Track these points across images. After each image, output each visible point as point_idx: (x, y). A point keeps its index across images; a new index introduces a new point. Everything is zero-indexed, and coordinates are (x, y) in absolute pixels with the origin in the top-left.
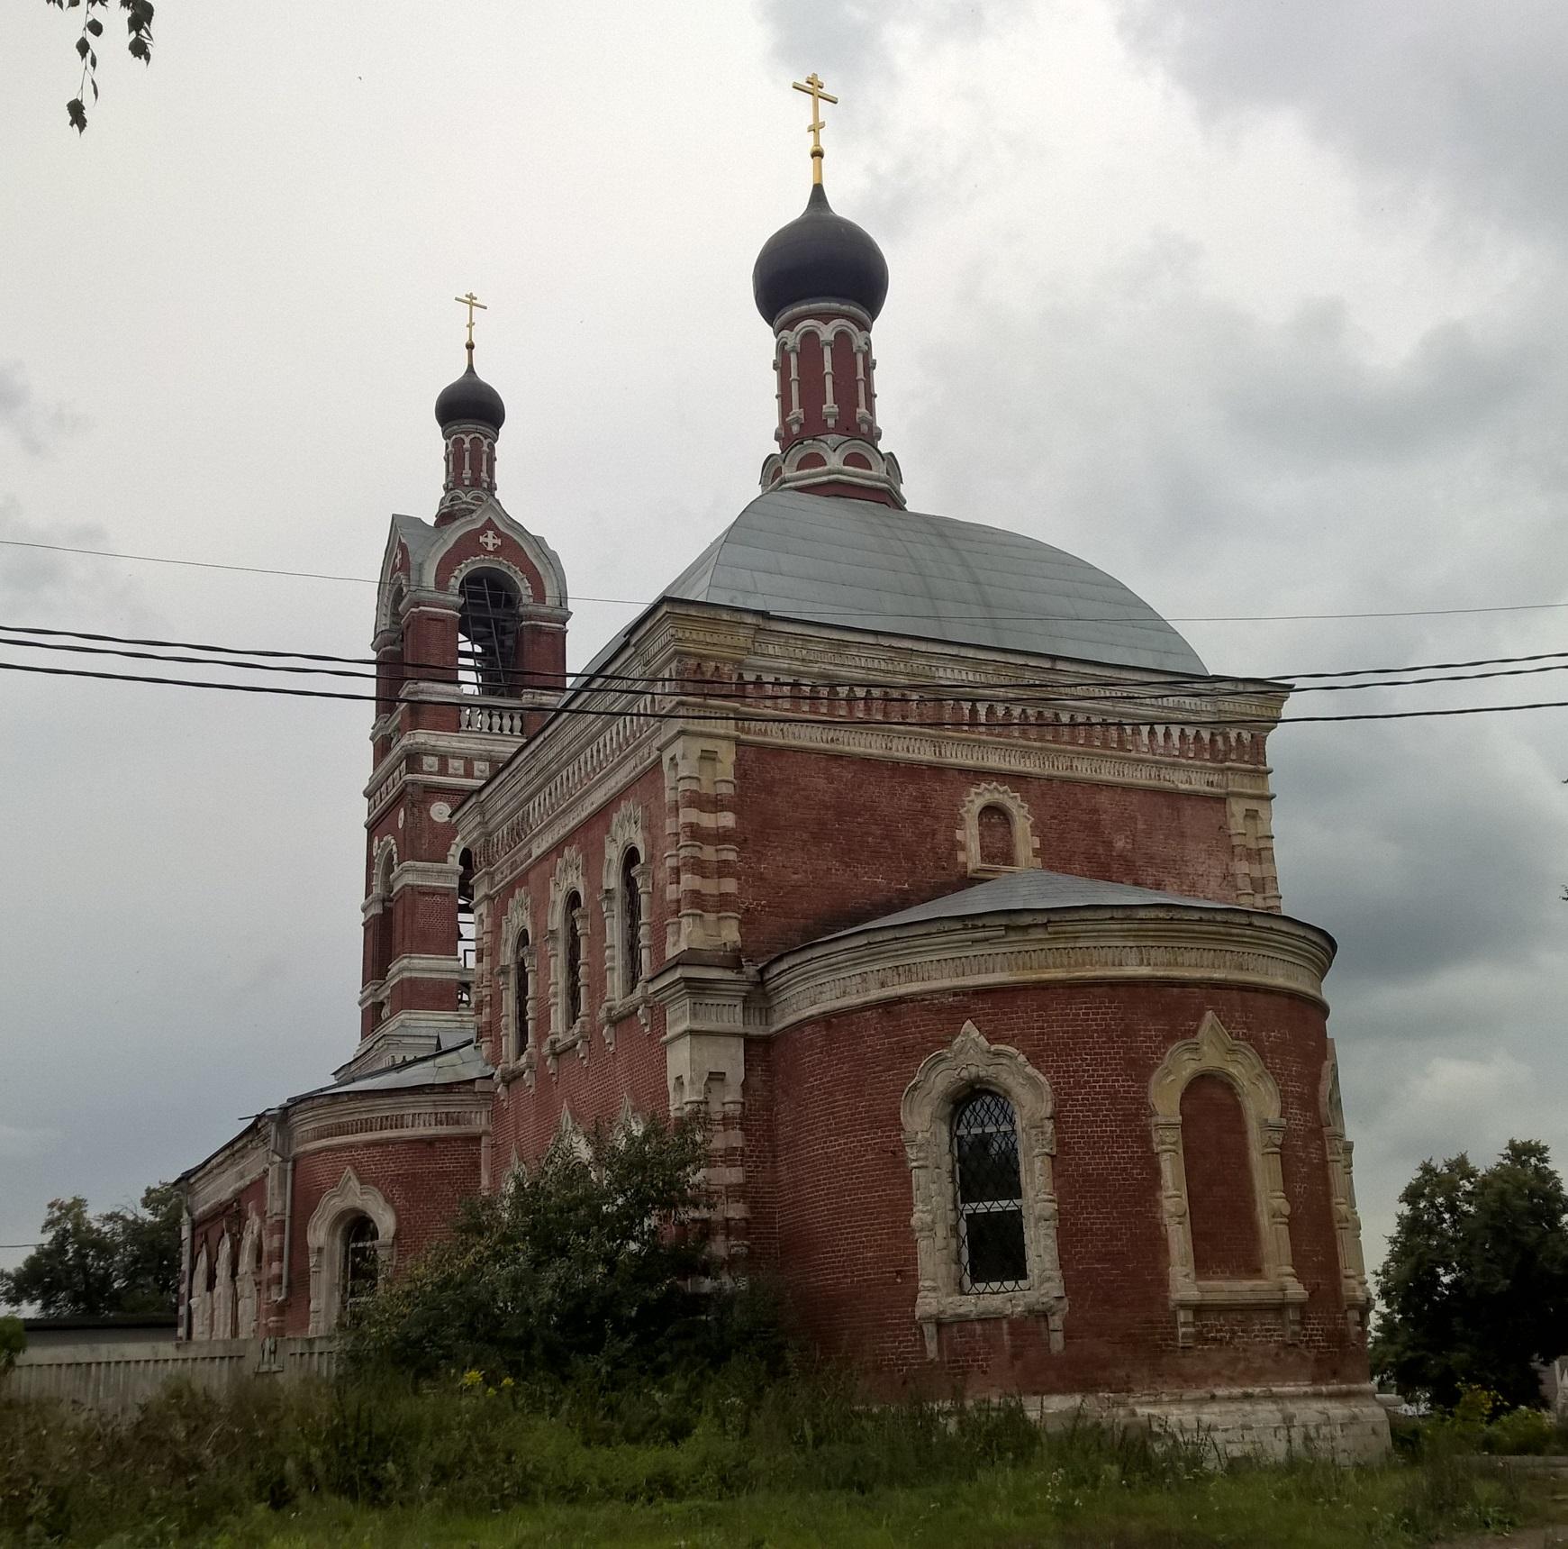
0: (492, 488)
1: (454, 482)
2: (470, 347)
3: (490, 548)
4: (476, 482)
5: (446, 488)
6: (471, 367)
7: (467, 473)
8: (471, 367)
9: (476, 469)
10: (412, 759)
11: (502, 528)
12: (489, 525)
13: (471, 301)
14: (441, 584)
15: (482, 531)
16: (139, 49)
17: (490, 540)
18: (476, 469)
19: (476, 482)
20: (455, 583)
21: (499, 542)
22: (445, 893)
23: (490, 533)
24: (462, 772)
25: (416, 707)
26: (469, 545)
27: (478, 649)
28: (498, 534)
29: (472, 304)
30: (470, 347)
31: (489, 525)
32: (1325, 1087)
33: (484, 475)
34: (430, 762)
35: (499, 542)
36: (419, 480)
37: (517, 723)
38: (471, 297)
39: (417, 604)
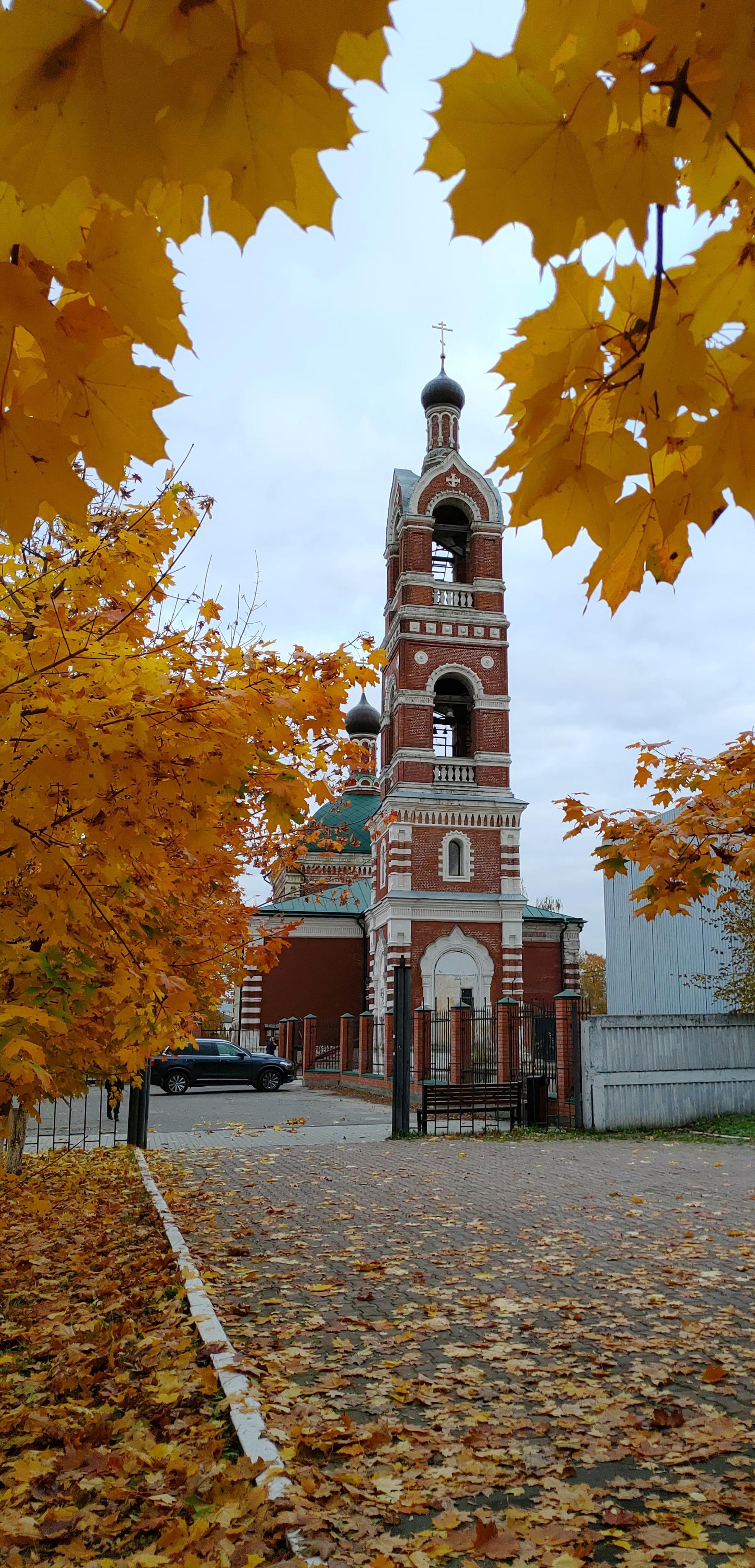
0: (456, 448)
1: (433, 445)
2: (443, 357)
3: (453, 485)
4: (446, 443)
5: (429, 450)
6: (443, 369)
7: (440, 438)
8: (443, 369)
9: (446, 435)
10: (404, 624)
11: (462, 471)
12: (454, 469)
13: (442, 327)
14: (422, 509)
15: (448, 474)
16: (443, 397)
17: (453, 480)
18: (446, 435)
19: (446, 443)
20: (431, 508)
21: (459, 481)
22: (424, 708)
23: (453, 475)
24: (434, 631)
25: (406, 590)
26: (440, 483)
27: (451, 555)
28: (459, 475)
29: (442, 329)
30: (443, 357)
31: (454, 469)
32: (347, 121)
33: (451, 439)
34: (414, 626)
35: (459, 481)
36: (411, 450)
37: (470, 599)
38: (442, 324)
39: (406, 524)
